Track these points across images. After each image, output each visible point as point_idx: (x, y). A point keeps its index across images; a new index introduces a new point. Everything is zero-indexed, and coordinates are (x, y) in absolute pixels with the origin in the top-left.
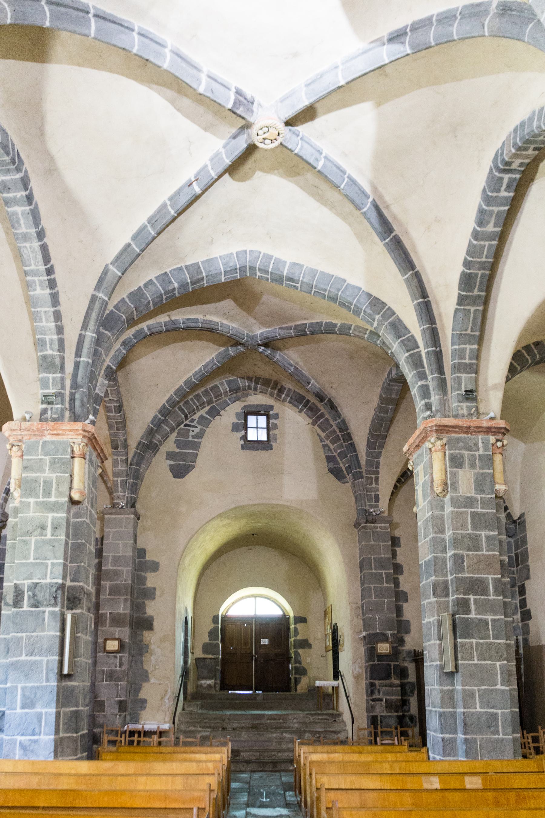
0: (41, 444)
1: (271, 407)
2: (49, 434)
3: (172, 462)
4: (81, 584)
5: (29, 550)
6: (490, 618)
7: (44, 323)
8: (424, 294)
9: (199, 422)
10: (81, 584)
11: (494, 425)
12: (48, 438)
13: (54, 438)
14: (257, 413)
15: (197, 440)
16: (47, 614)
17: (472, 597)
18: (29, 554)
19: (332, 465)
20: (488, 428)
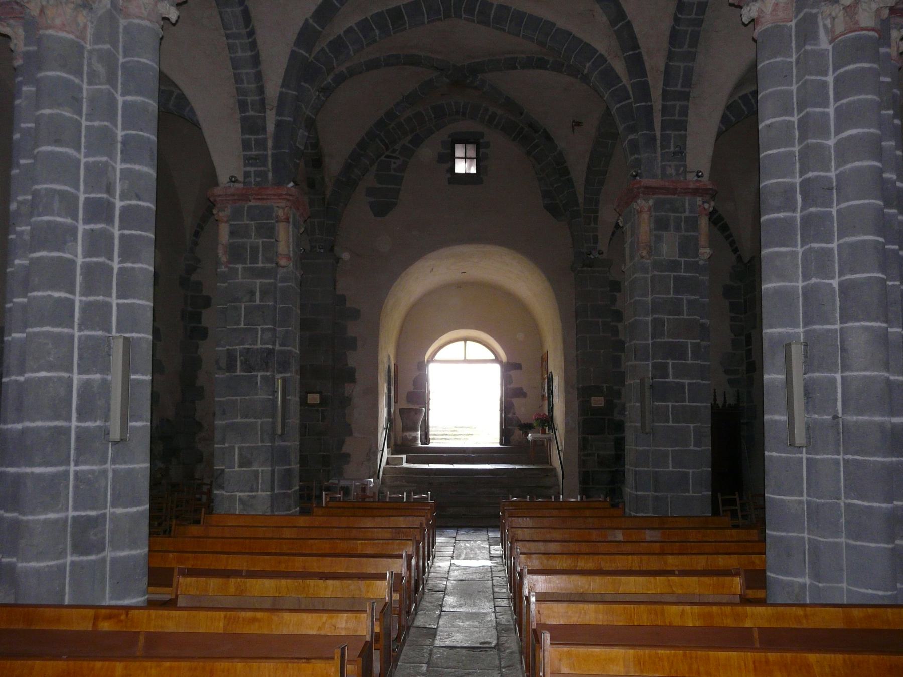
1: (482, 135)
4: (289, 348)
5: (239, 315)
6: (686, 381)
7: (245, 85)
10: (289, 348)
12: (253, 203)
13: (258, 203)
16: (259, 377)
17: (670, 362)
18: (240, 320)
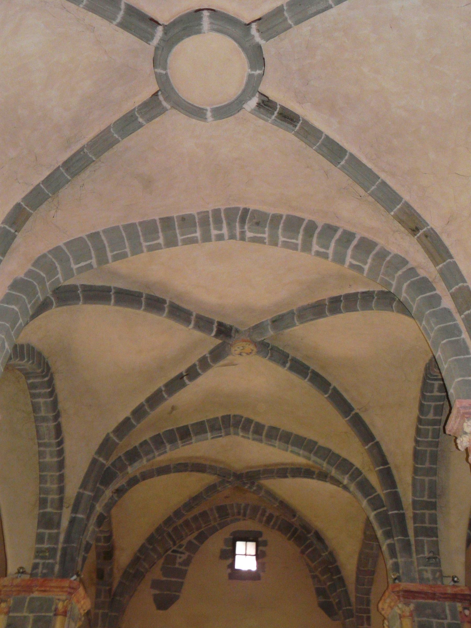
0: (28, 600)
2: (37, 590)
3: (157, 592)
8: (384, 461)
9: (187, 549)
11: (460, 592)
12: (36, 595)
14: (246, 539)
15: (183, 568)
19: (322, 599)
20: (453, 594)
